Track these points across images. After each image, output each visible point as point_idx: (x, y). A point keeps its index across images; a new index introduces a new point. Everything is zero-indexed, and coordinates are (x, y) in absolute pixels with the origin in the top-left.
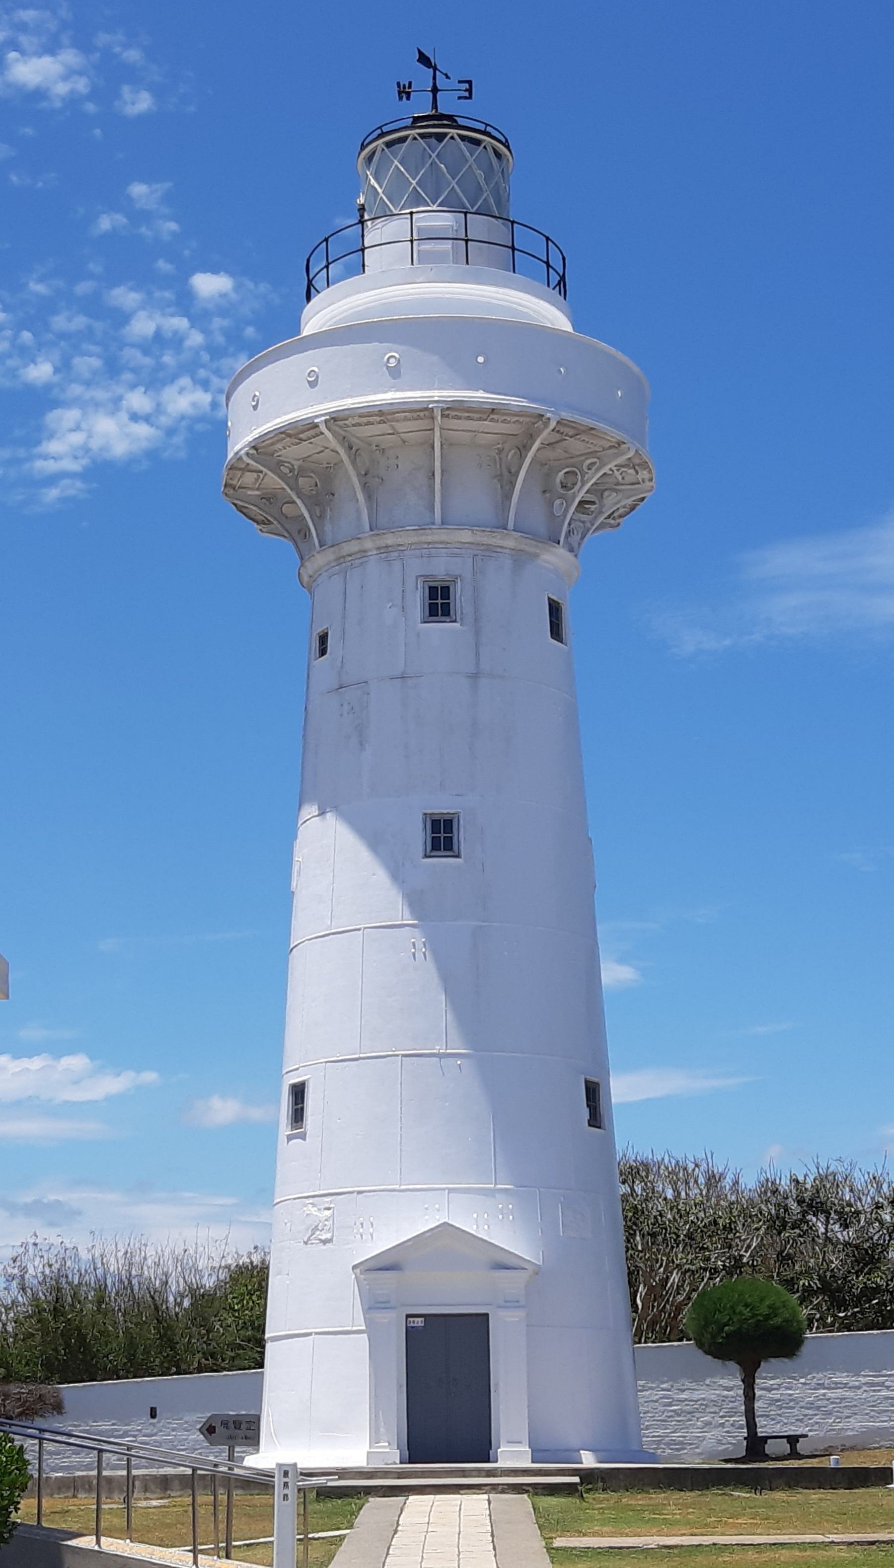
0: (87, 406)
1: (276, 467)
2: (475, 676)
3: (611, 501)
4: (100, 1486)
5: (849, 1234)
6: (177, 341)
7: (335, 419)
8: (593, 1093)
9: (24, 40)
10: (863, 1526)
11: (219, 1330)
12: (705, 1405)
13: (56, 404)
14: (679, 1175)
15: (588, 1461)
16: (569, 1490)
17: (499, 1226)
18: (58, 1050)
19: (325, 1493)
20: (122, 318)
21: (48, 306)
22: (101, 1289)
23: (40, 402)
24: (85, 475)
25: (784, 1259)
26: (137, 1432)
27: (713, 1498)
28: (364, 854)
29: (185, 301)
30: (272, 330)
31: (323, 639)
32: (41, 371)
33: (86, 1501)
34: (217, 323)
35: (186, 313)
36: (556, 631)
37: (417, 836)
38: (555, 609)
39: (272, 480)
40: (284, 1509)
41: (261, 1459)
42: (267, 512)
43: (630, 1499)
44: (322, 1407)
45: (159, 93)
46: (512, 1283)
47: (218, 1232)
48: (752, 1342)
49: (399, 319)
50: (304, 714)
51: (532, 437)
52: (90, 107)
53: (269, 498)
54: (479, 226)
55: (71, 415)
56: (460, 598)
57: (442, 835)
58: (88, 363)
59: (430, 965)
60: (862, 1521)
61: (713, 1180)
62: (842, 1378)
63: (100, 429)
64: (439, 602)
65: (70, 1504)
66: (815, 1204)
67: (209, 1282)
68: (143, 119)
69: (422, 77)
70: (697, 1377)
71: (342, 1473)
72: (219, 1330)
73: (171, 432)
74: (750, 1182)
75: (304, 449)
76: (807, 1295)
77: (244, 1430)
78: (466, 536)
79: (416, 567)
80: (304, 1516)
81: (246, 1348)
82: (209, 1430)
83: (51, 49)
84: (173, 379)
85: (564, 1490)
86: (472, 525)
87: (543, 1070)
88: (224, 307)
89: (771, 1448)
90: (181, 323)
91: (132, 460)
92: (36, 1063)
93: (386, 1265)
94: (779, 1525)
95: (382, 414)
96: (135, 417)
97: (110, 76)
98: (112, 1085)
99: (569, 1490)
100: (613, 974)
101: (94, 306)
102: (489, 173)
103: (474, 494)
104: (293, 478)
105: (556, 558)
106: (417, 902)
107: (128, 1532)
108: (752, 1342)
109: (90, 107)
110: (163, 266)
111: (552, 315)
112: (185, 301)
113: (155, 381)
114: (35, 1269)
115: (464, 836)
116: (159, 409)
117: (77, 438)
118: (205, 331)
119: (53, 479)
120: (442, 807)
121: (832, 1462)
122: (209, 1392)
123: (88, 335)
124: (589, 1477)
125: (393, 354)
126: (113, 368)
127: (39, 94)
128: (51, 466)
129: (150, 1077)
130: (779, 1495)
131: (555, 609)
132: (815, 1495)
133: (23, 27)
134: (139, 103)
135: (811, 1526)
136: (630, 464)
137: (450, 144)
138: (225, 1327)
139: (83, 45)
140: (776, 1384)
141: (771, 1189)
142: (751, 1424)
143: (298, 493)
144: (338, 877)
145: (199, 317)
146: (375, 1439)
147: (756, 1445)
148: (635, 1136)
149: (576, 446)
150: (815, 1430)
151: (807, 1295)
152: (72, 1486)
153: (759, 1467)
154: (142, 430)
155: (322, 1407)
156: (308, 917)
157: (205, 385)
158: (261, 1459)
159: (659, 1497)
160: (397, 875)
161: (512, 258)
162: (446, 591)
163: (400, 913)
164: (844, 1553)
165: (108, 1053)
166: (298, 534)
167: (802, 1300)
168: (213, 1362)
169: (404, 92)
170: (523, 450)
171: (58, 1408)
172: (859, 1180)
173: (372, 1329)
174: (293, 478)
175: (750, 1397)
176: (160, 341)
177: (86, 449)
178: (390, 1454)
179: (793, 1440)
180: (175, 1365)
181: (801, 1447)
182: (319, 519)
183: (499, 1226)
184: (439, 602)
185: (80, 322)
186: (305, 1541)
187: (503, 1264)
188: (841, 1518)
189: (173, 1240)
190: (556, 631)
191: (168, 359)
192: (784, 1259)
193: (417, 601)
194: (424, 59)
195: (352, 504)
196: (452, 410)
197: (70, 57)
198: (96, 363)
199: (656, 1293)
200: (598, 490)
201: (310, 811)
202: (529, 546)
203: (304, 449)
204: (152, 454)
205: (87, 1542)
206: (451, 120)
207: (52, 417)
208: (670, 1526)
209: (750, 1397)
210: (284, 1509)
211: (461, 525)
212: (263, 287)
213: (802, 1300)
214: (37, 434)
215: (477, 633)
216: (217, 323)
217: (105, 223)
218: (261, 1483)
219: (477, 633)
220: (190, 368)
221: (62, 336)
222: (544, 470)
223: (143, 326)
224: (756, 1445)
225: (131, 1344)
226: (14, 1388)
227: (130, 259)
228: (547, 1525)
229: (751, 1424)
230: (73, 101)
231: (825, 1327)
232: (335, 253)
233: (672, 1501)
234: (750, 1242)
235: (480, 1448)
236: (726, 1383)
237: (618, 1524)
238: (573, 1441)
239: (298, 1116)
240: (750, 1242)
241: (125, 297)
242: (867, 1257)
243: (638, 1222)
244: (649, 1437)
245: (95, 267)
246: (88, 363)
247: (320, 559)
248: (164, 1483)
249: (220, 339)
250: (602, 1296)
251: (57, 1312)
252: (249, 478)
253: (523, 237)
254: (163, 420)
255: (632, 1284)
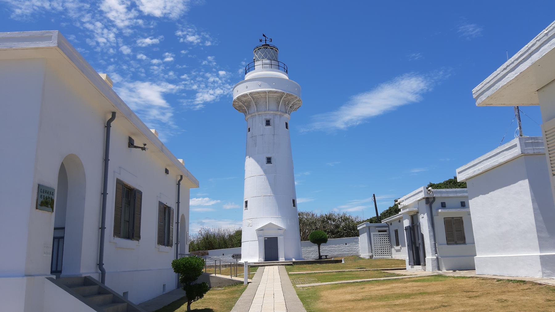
0: (203, 93)
1: (241, 101)
2: (274, 135)
3: (295, 107)
4: (216, 266)
5: (333, 223)
6: (217, 82)
7: (251, 94)
8: (294, 201)
9: (189, 34)
10: (338, 269)
11: (234, 241)
12: (312, 251)
13: (198, 92)
14: (307, 214)
15: (294, 260)
16: (291, 265)
17: (279, 223)
18: (204, 197)
19: (252, 266)
20: (208, 78)
21: (196, 77)
22: (214, 235)
23: (195, 92)
24: (203, 104)
25: (324, 227)
26: (221, 257)
27: (314, 265)
28: (256, 164)
29: (218, 75)
30: (237, 80)
31: (249, 129)
32: (195, 87)
33: (213, 269)
34: (223, 79)
35: (218, 77)
36: (287, 127)
37: (265, 161)
38: (286, 124)
39: (241, 104)
40: (246, 269)
41: (242, 261)
42: (240, 109)
43: (302, 266)
44: (251, 252)
45: (212, 42)
46: (281, 232)
47: (233, 226)
48: (319, 240)
49: (260, 77)
50: (110, 157)
51: (282, 96)
52: (201, 44)
53: (240, 106)
54: (273, 62)
55: (200, 94)
56: (271, 122)
57: (269, 160)
58: (203, 86)
59: (267, 181)
60: (338, 268)
61: (313, 215)
62: (334, 246)
63: (206, 96)
64: (268, 123)
65: (210, 269)
66: (329, 218)
67: (232, 234)
68: (209, 46)
69: (264, 38)
70: (311, 246)
71: (255, 263)
72: (234, 241)
73: (217, 97)
74: (319, 215)
75: (245, 99)
76: (328, 232)
77: (239, 256)
78: (272, 112)
79: (264, 117)
80: (249, 270)
81: (239, 244)
82: (233, 256)
83: (194, 35)
84: (217, 88)
85: (290, 265)
86: (273, 111)
87: (286, 198)
88: (224, 76)
89: (323, 257)
90: (217, 79)
91: (211, 101)
92: (200, 199)
93: (261, 230)
94: (324, 269)
95: (258, 93)
96: (211, 94)
97: (204, 40)
98: (213, 202)
99: (291, 265)
100: (296, 183)
101: (203, 76)
102: (275, 53)
103: (273, 106)
104: (244, 103)
105: (287, 116)
106: (265, 172)
107: (220, 273)
108: (319, 240)
109: (201, 44)
110: (214, 70)
111: (285, 77)
112: (218, 75)
113: (214, 88)
114: (203, 232)
115: (272, 161)
116: (214, 93)
117: (201, 98)
118: (222, 80)
119: (198, 105)
120: (269, 156)
121: (333, 259)
122: (234, 250)
123: (202, 81)
124: (294, 263)
125: (260, 83)
126: (207, 87)
127: (192, 42)
128: (197, 103)
129: (219, 201)
130: (324, 265)
131: (286, 124)
132: (330, 264)
133: (189, 32)
134: (208, 44)
135: (330, 269)
136: (298, 100)
137: (269, 49)
138: (235, 241)
139: (199, 35)
140: (323, 247)
141: (322, 216)
142: (319, 254)
143: (245, 105)
144: (252, 168)
145: (220, 79)
146: (259, 258)
147: (320, 257)
148: (300, 208)
149: (289, 98)
150: (330, 254)
151: (328, 232)
152: (211, 267)
153: (321, 260)
154: (212, 96)
155: (251, 252)
156: (248, 174)
157: (222, 89)
158: (242, 261)
159: (305, 265)
160: (262, 167)
161: (278, 67)
162: (269, 121)
163: (262, 173)
164: (335, 273)
165: (212, 197)
166: (245, 112)
167: (328, 234)
168: (233, 246)
169: (261, 41)
170: (281, 98)
171: (208, 254)
172: (336, 214)
173: (259, 240)
174: (244, 103)
175: (319, 249)
176: (214, 82)
177: (203, 99)
178: (262, 260)
179: (326, 256)
180: (226, 247)
181: (328, 257)
182: (248, 110)
183: (279, 223)
184: (268, 123)
185: (201, 79)
186: (249, 274)
187: (280, 229)
188: (334, 268)
189: (226, 227)
190: (287, 127)
191: (216, 85)
192: (324, 227)
193: (264, 123)
194: (264, 35)
195: (254, 108)
196: (270, 92)
197: (197, 36)
198: (204, 85)
199: (304, 233)
200: (293, 105)
201: (247, 157)
202: (282, 114)
203: (245, 99)
204: (214, 100)
205: (214, 275)
206: (268, 45)
207: (197, 95)
208: (307, 270)
209: (319, 249)
210: (246, 269)
211: (271, 111)
212: (231, 73)
213: (328, 234)
214: (194, 98)
215: (274, 127)
216: (223, 79)
217: (204, 63)
218: (242, 265)
219: (274, 127)
220: (219, 86)
221: (198, 81)
222: (284, 101)
223: (211, 79)
224: (320, 257)
225: (219, 244)
226: (200, 251)
227: (208, 69)
228: (288, 270)
229: (319, 254)
230: (198, 43)
231: (331, 238)
232: (250, 68)
233: (307, 266)
234: (319, 225)
235: (277, 259)
236: (316, 247)
237: (299, 270)
238: (291, 257)
239: (246, 206)
240: (319, 225)
241: (208, 75)
242: (337, 226)
243: (300, 221)
244: (303, 256)
245: (203, 70)
246: (203, 86)
247: (249, 116)
248: (226, 266)
249: (224, 82)
250: (296, 234)
251: (207, 239)
252: (237, 103)
253: (280, 64)
254: (216, 95)
255: (300, 232)
